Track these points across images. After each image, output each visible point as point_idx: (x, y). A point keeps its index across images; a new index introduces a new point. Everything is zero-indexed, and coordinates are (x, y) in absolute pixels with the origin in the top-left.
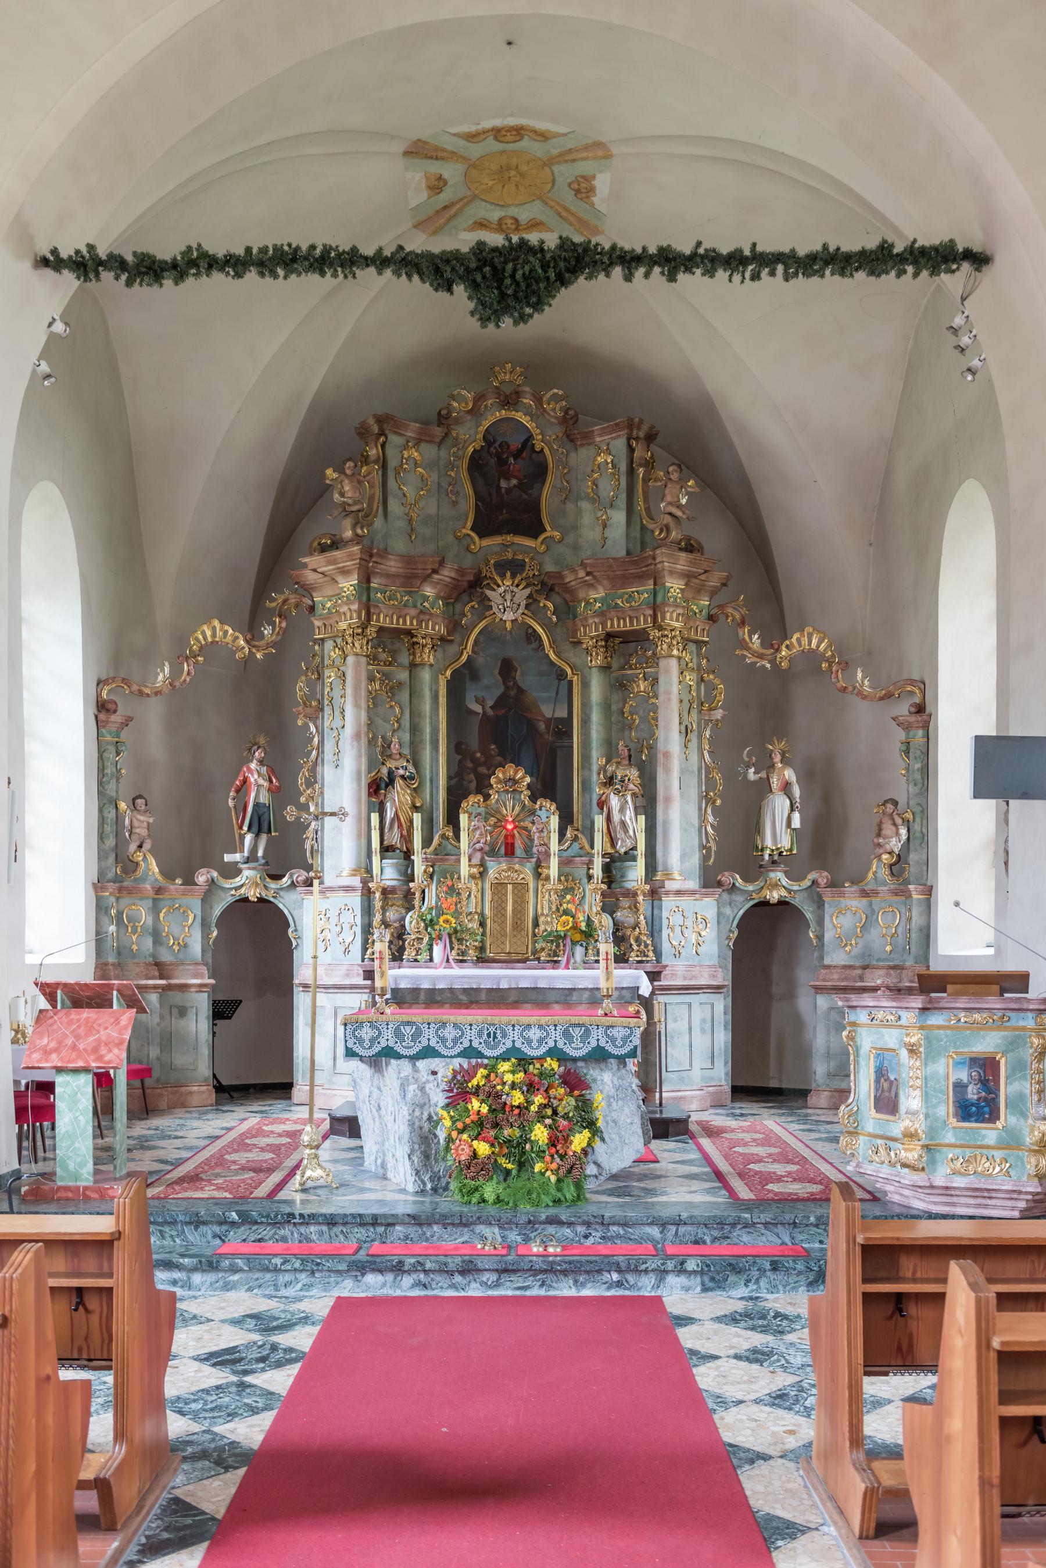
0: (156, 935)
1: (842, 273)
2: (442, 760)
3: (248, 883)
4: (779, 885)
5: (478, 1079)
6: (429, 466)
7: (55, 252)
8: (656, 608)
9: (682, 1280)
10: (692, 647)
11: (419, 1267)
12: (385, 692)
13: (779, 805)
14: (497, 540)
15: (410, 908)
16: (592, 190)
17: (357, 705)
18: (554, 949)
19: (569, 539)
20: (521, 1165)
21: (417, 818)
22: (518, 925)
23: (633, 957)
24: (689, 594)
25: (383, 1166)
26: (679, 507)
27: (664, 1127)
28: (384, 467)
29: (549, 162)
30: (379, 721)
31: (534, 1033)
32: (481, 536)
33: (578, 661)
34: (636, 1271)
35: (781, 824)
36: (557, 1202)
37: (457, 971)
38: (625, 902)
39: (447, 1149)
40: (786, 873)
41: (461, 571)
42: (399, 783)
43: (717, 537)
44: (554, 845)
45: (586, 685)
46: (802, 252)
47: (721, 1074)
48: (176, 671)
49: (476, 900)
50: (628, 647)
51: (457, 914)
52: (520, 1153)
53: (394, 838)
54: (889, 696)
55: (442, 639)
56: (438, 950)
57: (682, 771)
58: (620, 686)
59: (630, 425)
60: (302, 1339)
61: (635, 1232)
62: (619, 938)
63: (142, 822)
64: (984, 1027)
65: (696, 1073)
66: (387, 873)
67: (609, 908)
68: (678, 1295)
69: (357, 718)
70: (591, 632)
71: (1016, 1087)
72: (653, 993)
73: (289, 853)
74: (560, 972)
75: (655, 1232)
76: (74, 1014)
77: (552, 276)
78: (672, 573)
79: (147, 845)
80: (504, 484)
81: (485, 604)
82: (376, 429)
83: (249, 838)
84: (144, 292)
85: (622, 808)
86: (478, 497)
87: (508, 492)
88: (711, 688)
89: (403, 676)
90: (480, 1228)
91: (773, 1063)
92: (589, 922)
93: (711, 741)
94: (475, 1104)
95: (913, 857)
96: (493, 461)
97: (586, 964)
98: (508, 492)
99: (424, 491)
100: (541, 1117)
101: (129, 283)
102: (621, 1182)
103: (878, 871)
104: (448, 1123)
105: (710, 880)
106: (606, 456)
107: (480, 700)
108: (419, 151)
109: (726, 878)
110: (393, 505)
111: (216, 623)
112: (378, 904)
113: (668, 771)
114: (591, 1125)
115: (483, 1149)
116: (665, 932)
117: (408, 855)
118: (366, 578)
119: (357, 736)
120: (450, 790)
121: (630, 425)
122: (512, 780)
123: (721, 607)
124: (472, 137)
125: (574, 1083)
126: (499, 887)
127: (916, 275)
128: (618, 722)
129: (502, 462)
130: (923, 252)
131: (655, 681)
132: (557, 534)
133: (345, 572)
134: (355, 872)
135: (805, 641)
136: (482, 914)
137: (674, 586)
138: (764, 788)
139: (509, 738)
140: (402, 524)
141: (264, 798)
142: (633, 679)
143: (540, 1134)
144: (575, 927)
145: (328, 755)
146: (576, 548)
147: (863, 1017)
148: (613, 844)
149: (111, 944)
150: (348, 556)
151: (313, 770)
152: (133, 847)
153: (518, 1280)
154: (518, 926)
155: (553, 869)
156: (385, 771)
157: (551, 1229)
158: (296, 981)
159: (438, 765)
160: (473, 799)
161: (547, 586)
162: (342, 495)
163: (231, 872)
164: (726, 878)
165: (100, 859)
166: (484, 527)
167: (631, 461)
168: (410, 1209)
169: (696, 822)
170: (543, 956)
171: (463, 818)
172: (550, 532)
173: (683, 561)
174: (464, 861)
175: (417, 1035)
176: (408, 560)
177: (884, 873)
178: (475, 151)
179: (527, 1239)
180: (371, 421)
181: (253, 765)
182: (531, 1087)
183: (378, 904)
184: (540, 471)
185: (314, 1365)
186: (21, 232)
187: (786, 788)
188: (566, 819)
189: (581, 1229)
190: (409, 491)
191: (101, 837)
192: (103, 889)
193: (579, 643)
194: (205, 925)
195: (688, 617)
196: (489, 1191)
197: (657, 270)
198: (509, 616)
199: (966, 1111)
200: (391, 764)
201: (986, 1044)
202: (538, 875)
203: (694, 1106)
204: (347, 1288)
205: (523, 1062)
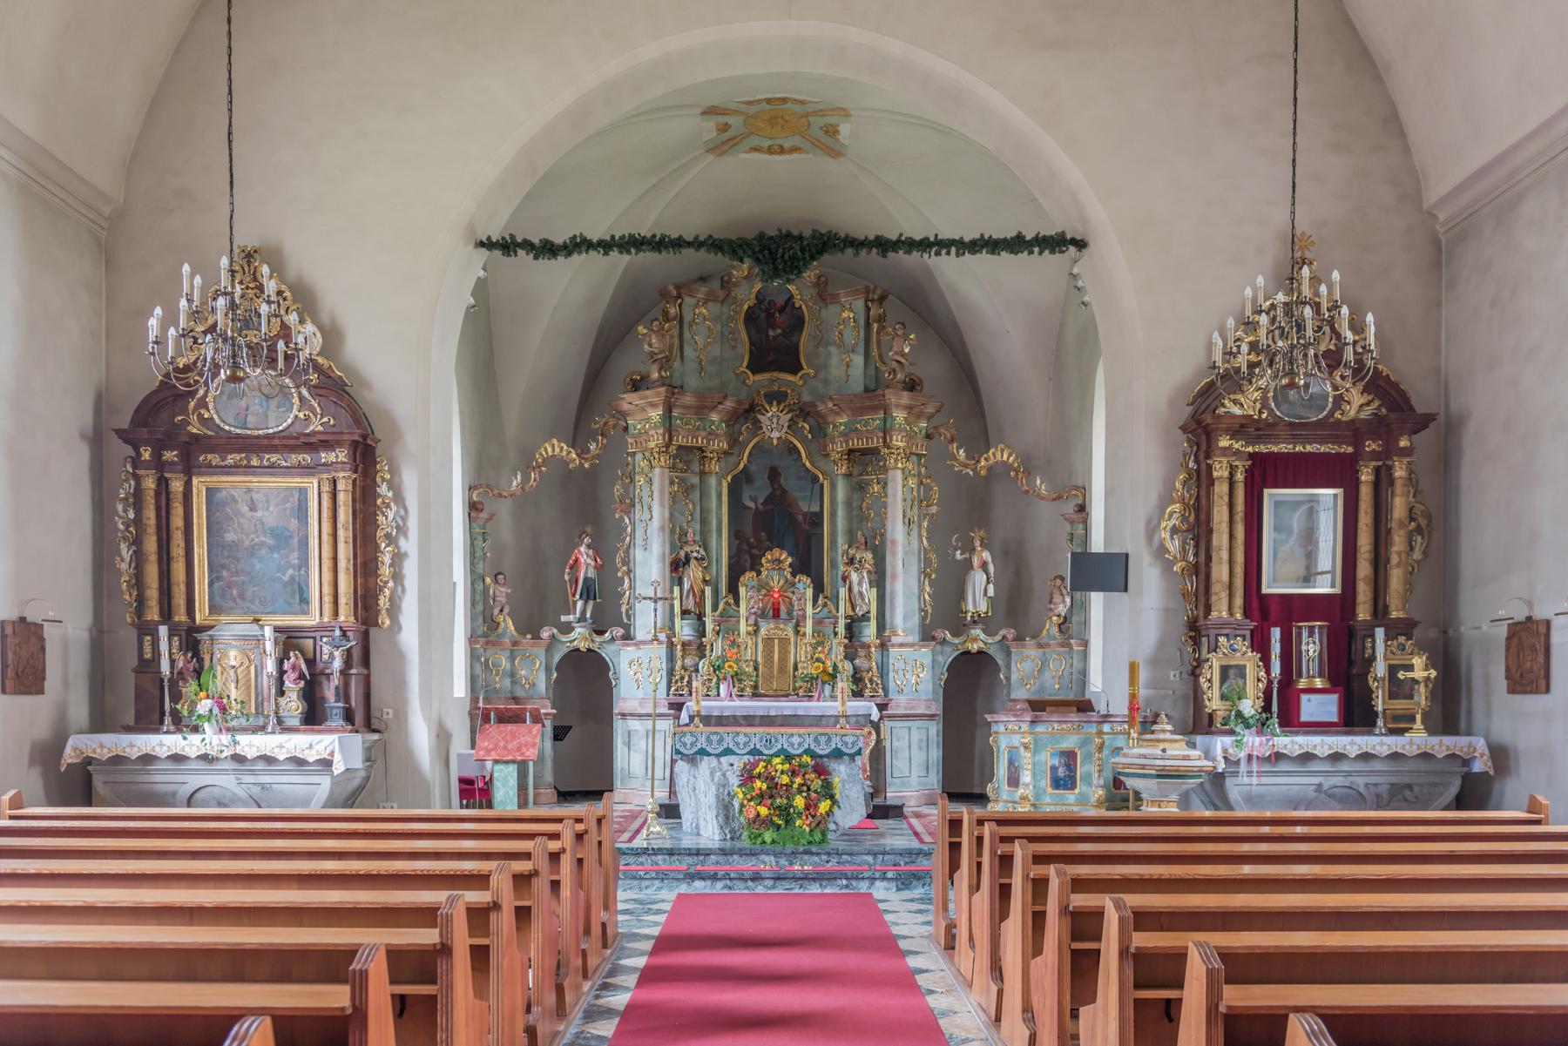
0: (513, 675)
1: (993, 253)
2: (725, 544)
3: (579, 637)
4: (978, 640)
5: (760, 769)
6: (715, 319)
7: (489, 238)
8: (886, 432)
9: (885, 884)
10: (914, 458)
11: (727, 877)
12: (683, 491)
13: (978, 579)
14: (767, 376)
15: (703, 656)
16: (837, 132)
17: (662, 505)
18: (811, 686)
19: (822, 376)
20: (787, 822)
21: (708, 590)
22: (782, 670)
23: (867, 693)
24: (911, 419)
25: (697, 827)
26: (903, 355)
27: (882, 811)
29: (807, 115)
31: (796, 740)
32: (754, 373)
34: (857, 878)
35: (979, 594)
36: (810, 843)
37: (738, 703)
38: (862, 652)
39: (741, 811)
40: (984, 631)
41: (739, 402)
42: (693, 563)
43: (934, 369)
44: (809, 610)
45: (833, 487)
46: (967, 239)
47: (934, 780)
48: (526, 479)
49: (751, 651)
50: (865, 461)
51: (737, 661)
52: (786, 813)
53: (690, 604)
54: (1059, 498)
55: (725, 453)
56: (723, 688)
57: (906, 553)
58: (860, 488)
59: (867, 291)
60: (667, 907)
61: (858, 859)
62: (857, 678)
63: (502, 592)
64: (1068, 732)
65: (914, 779)
66: (684, 630)
67: (850, 657)
68: (880, 891)
69: (662, 514)
70: (837, 447)
71: (1086, 768)
72: (881, 718)
73: (608, 614)
74: (814, 704)
75: (870, 859)
76: (502, 727)
77: (807, 255)
78: (897, 406)
79: (506, 610)
80: (771, 333)
82: (675, 293)
83: (580, 604)
84: (544, 263)
85: (860, 582)
87: (775, 343)
88: (929, 489)
89: (695, 480)
90: (763, 857)
91: (976, 775)
92: (835, 667)
94: (758, 784)
95: (1075, 619)
96: (763, 315)
97: (833, 698)
98: (775, 343)
99: (711, 336)
100: (800, 791)
101: (536, 258)
102: (851, 834)
103: (1051, 628)
104: (741, 796)
105: (927, 636)
106: (848, 313)
107: (754, 497)
108: (711, 111)
109: (939, 634)
110: (688, 352)
111: (555, 441)
112: (679, 654)
113: (894, 554)
114: (832, 797)
115: (763, 811)
116: (891, 675)
117: (700, 616)
118: (669, 409)
119: (662, 528)
120: (731, 567)
122: (777, 565)
123: (936, 428)
124: (749, 103)
125: (820, 771)
126: (768, 641)
127: (1040, 253)
128: (857, 516)
129: (770, 316)
130: (1045, 239)
132: (812, 372)
133: (653, 405)
135: (999, 454)
136: (756, 661)
137: (899, 416)
138: (968, 565)
139: (775, 527)
140: (694, 365)
141: (592, 574)
142: (869, 483)
143: (799, 802)
144: (825, 671)
145: (639, 541)
146: (826, 382)
147: (1002, 728)
148: (853, 609)
149: (480, 682)
150: (657, 395)
151: (627, 552)
152: (496, 611)
153: (786, 884)
154: (782, 670)
155: (808, 628)
156: (682, 554)
157: (806, 857)
158: (616, 711)
159: (721, 547)
160: (749, 575)
161: (803, 412)
162: (650, 345)
163: (567, 628)
164: (939, 634)
165: (472, 620)
166: (755, 367)
168: (717, 845)
169: (916, 591)
170: (801, 692)
171: (742, 590)
172: (806, 370)
173: (906, 398)
174: (743, 622)
175: (721, 741)
176: (700, 395)
177: (1055, 630)
178: (752, 109)
179: (791, 864)
180: (671, 287)
181: (582, 549)
182: (794, 773)
183: (679, 654)
184: (799, 323)
185: (673, 914)
186: (471, 228)
187: (984, 565)
188: (819, 588)
189: (824, 857)
191: (473, 604)
192: (476, 642)
193: (828, 455)
194: (548, 669)
195: (910, 437)
196: (768, 836)
197: (874, 250)
198: (775, 435)
199: (1057, 783)
200: (687, 549)
201: (1070, 743)
202: (797, 632)
203: (912, 803)
204: (684, 888)
205: (789, 758)
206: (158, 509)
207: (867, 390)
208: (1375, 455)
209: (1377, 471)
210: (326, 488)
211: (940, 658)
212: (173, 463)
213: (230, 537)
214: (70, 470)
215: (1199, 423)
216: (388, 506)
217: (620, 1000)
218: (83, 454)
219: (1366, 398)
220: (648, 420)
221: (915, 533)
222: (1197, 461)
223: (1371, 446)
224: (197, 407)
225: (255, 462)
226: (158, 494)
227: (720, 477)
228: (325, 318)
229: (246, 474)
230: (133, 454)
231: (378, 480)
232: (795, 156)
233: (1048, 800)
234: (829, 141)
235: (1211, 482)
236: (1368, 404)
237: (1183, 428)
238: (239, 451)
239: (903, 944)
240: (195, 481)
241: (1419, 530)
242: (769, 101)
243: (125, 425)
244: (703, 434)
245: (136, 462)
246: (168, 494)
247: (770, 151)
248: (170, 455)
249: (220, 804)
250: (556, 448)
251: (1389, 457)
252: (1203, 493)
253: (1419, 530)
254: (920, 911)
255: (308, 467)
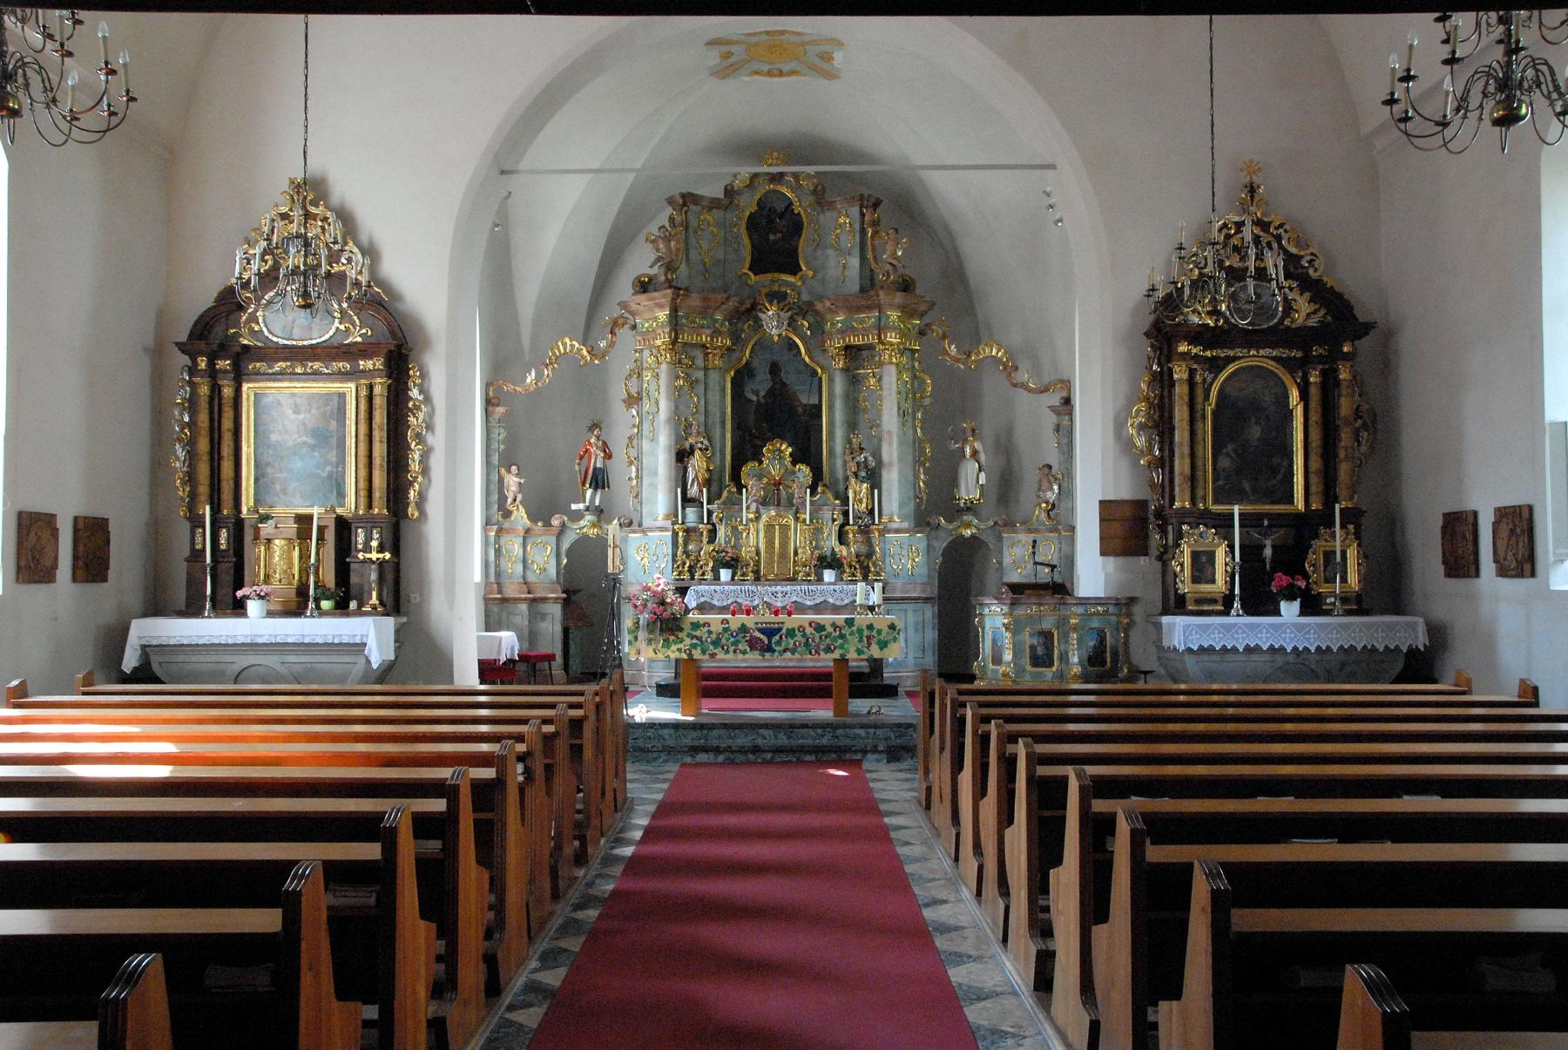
2: (728, 436)
9: (876, 756)
10: (908, 353)
14: (769, 276)
17: (669, 399)
19: (819, 277)
22: (783, 555)
26: (897, 258)
28: (687, 228)
29: (803, 44)
30: (682, 407)
33: (825, 363)
42: (697, 454)
45: (831, 380)
47: (930, 660)
55: (728, 349)
58: (854, 381)
60: (671, 776)
80: (772, 237)
81: (758, 324)
86: (753, 246)
89: (700, 374)
93: (923, 421)
95: (1063, 505)
106: (844, 220)
107: (758, 388)
110: (694, 255)
118: (674, 310)
119: (669, 421)
121: (862, 198)
122: (777, 457)
126: (769, 528)
129: (771, 221)
131: (880, 380)
132: (810, 273)
133: (661, 306)
134: (667, 517)
146: (823, 281)
161: (805, 310)
163: (577, 516)
166: (758, 266)
167: (863, 222)
173: (899, 298)
177: (1043, 516)
178: (754, 39)
184: (797, 227)
190: (705, 244)
193: (825, 351)
194: (558, 556)
202: (797, 519)
206: (211, 412)
207: (863, 290)
208: (1320, 359)
209: (1324, 373)
210: (364, 392)
211: (935, 544)
212: (226, 372)
213: (274, 437)
214: (134, 379)
215: (1159, 331)
216: (418, 408)
217: (628, 851)
218: (146, 362)
219: (1314, 307)
220: (656, 319)
221: (909, 424)
222: (1159, 364)
223: (1316, 351)
224: (248, 321)
225: (299, 370)
226: (211, 398)
227: (724, 371)
228: (364, 239)
229: (291, 380)
230: (189, 363)
231: (411, 384)
232: (794, 78)
233: (1028, 677)
234: (825, 66)
235: (1172, 384)
236: (1315, 312)
237: (1147, 334)
238: (285, 360)
239: (883, 807)
240: (245, 387)
241: (1365, 426)
242: (768, 33)
243: (183, 337)
244: (708, 331)
245: (193, 370)
246: (220, 398)
247: (770, 74)
248: (224, 364)
249: (264, 682)
250: (570, 344)
251: (1335, 361)
252: (1166, 393)
253: (1365, 426)
254: (907, 780)
255: (346, 374)
